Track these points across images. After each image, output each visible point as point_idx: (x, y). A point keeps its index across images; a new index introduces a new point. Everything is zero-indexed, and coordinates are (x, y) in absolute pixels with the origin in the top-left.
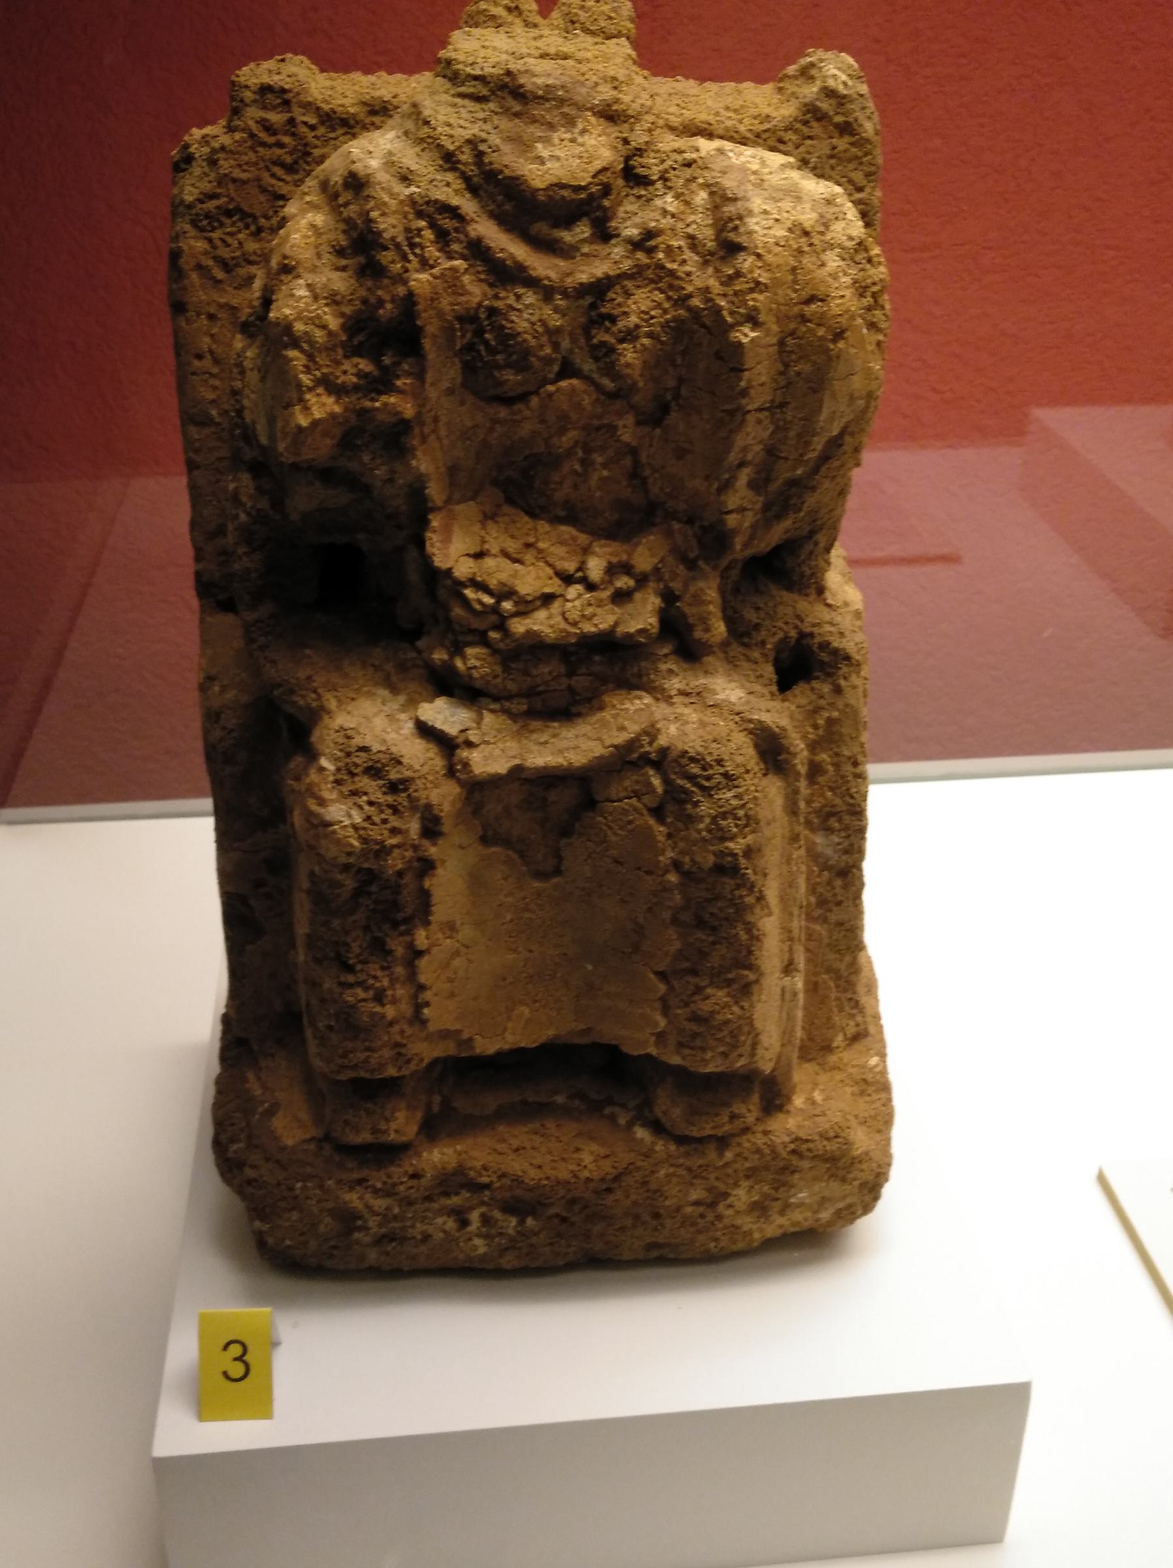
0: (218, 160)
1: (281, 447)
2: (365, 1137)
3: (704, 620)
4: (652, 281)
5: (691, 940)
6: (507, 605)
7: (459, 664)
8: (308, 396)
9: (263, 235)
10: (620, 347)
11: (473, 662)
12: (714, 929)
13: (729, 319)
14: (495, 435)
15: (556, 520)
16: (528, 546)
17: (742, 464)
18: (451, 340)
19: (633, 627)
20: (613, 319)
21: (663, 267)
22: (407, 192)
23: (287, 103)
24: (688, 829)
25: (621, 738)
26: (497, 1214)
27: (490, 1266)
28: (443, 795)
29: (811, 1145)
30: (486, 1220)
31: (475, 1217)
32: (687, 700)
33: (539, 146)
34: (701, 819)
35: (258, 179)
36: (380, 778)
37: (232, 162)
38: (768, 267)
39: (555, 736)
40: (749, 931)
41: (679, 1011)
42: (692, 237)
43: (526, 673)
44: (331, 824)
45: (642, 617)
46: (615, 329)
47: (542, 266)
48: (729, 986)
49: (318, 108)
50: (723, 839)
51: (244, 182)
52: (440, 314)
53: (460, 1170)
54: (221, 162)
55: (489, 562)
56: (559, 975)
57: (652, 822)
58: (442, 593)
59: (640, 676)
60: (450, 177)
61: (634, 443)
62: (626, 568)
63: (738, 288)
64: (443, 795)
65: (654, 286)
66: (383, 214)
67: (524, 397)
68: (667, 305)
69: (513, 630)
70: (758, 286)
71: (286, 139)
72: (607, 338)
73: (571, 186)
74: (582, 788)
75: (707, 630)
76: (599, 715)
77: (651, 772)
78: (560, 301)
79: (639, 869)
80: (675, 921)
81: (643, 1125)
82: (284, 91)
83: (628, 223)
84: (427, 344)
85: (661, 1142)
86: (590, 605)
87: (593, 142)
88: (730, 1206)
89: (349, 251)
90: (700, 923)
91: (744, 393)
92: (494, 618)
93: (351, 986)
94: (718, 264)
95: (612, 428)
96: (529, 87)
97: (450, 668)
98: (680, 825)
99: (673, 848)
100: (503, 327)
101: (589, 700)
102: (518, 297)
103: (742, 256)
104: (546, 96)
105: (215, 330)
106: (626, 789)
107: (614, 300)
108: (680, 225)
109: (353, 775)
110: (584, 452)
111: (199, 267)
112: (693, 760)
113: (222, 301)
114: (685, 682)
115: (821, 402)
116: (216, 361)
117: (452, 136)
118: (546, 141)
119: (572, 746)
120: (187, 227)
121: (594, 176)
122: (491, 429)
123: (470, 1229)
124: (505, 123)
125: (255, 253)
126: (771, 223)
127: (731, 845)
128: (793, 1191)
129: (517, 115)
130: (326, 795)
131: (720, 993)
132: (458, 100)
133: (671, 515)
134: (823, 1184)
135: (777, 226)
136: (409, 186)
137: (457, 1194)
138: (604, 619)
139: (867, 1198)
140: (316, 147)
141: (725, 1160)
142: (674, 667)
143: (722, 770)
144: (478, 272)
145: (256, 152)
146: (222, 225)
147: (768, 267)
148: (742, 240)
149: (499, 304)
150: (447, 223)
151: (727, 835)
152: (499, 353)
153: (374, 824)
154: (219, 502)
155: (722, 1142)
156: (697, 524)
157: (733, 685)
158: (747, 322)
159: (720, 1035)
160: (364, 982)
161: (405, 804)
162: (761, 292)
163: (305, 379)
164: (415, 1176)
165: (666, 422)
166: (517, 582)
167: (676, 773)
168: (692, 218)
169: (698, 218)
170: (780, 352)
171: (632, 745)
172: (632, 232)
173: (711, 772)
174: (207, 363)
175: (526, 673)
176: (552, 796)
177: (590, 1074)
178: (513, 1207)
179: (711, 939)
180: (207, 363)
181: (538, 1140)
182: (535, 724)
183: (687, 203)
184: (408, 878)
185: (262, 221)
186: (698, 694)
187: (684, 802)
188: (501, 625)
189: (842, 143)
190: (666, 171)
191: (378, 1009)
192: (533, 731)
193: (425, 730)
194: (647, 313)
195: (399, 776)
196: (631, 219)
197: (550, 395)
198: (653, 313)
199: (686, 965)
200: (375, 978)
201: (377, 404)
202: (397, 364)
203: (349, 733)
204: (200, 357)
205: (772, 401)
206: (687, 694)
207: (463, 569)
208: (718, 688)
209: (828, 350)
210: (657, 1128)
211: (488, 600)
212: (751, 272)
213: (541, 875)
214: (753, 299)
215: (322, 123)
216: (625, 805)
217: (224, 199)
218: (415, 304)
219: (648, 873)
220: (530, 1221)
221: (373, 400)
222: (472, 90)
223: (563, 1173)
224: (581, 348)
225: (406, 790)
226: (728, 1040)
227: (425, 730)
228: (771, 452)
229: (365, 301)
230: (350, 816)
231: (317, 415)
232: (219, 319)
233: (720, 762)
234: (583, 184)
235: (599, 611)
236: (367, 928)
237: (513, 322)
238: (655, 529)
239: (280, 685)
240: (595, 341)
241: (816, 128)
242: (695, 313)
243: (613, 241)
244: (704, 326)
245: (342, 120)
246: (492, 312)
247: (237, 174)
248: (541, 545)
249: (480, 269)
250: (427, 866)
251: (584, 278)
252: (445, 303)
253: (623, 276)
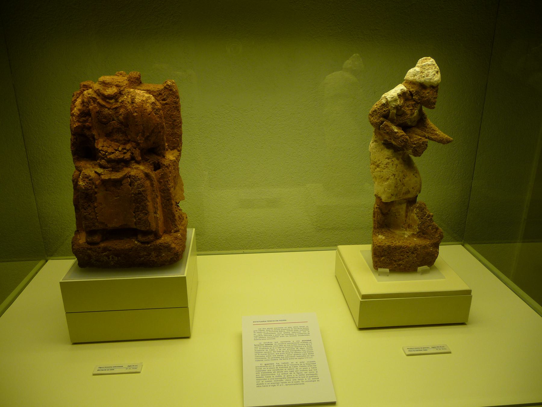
19: (126, 157)
30: (113, 258)
62: (125, 149)
70: (136, 108)
74: (117, 183)
104: (108, 84)
189: (171, 92)
207: (100, 148)
223: (123, 248)
227: (96, 172)
241: (166, 90)
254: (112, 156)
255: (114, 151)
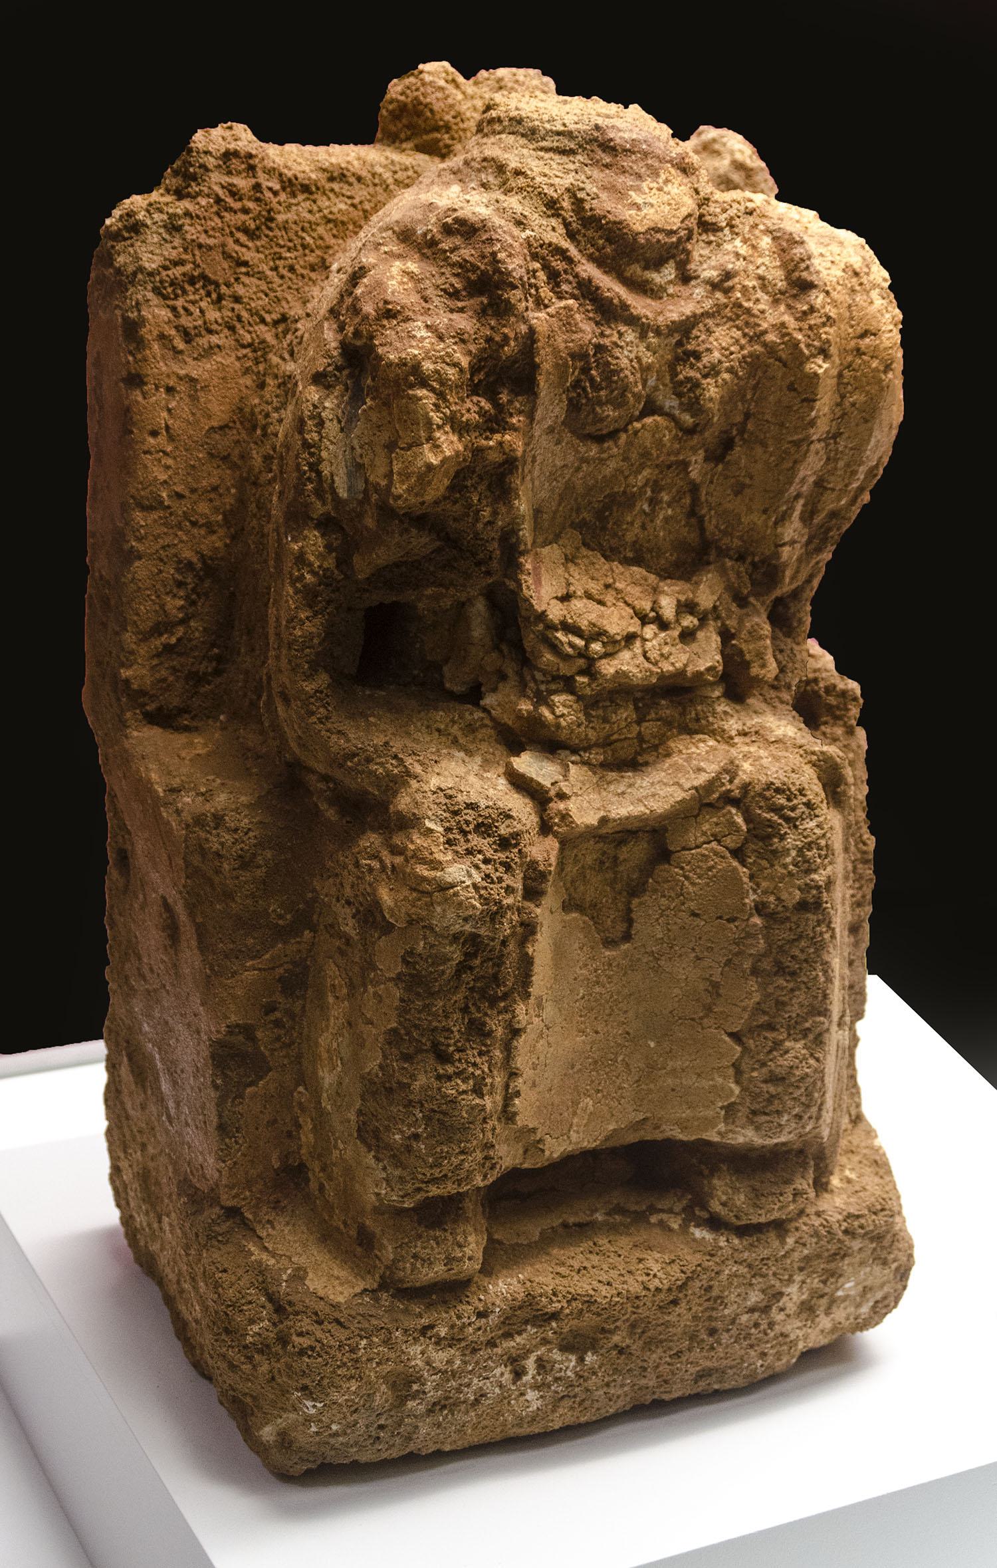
0: (183, 225)
1: (400, 489)
2: (437, 1271)
3: (760, 655)
4: (730, 319)
5: (770, 989)
6: (596, 647)
7: (546, 713)
8: (438, 434)
9: (224, 302)
10: (704, 382)
11: (560, 710)
12: (793, 974)
13: (806, 352)
14: (581, 475)
15: (627, 562)
16: (607, 586)
17: (797, 497)
18: (563, 376)
20: (697, 356)
21: (740, 306)
22: (524, 235)
23: (252, 168)
24: (772, 866)
25: (701, 779)
26: (556, 1355)
27: (536, 1429)
28: (543, 850)
29: (863, 1221)
30: (541, 1364)
31: (530, 1364)
32: (747, 740)
33: (631, 193)
34: (787, 852)
35: (223, 245)
36: (489, 836)
37: (199, 228)
38: (835, 304)
39: (630, 786)
40: (825, 972)
41: (755, 1074)
42: (761, 278)
43: (606, 720)
44: (452, 886)
45: (706, 655)
46: (700, 365)
47: (640, 306)
48: (805, 1036)
49: (281, 175)
50: (808, 871)
51: (210, 248)
52: (556, 351)
53: (531, 1299)
54: (187, 228)
55: (577, 604)
56: (620, 1059)
57: (735, 864)
58: (529, 641)
59: (698, 720)
60: (554, 222)
61: (698, 481)
63: (812, 322)
64: (543, 850)
65: (731, 323)
66: (510, 255)
67: (613, 435)
68: (743, 341)
69: (605, 672)
71: (251, 205)
72: (692, 374)
73: (663, 230)
74: (656, 839)
75: (763, 666)
76: (669, 761)
77: (734, 811)
78: (653, 339)
79: (720, 918)
80: (755, 971)
81: (697, 1226)
82: (250, 156)
83: (705, 266)
84: (542, 380)
85: (723, 1239)
86: (666, 644)
87: (676, 191)
88: (782, 1310)
89: (464, 293)
90: (781, 970)
91: (812, 423)
92: (581, 662)
93: (449, 1078)
94: (790, 302)
95: (685, 465)
96: (618, 141)
97: (535, 721)
98: (764, 863)
99: (755, 891)
100: (609, 364)
101: (655, 747)
102: (621, 335)
103: (814, 293)
105: (172, 405)
106: (704, 833)
107: (698, 337)
108: (751, 267)
109: (465, 833)
110: (653, 492)
111: (162, 337)
112: (778, 791)
113: (182, 372)
114: (740, 723)
115: (871, 430)
116: (171, 439)
117: (552, 185)
118: (638, 189)
119: (652, 793)
120: (150, 295)
121: (682, 222)
122: (578, 469)
123: (525, 1379)
124: (596, 173)
125: (216, 322)
126: (829, 265)
127: (816, 877)
128: (841, 1280)
129: (607, 166)
130: (440, 856)
131: (799, 1045)
132: (542, 154)
133: (723, 553)
134: (868, 1269)
135: (834, 267)
136: (524, 230)
137: (519, 1333)
138: (679, 659)
139: (899, 1287)
140: (279, 212)
141: (787, 1247)
142: (727, 709)
143: (804, 800)
144: (588, 311)
145: (222, 218)
146: (185, 292)
147: (835, 304)
148: (814, 278)
149: (606, 342)
150: (559, 265)
151: (813, 867)
152: (602, 389)
153: (493, 882)
154: (158, 597)
155: (780, 1227)
156: (749, 560)
157: (783, 722)
158: (819, 354)
159: (797, 1093)
160: (462, 1072)
161: (517, 860)
162: (831, 326)
163: (436, 418)
164: (481, 1315)
165: (728, 458)
166: (605, 622)
167: (760, 808)
168: (760, 261)
169: (767, 260)
170: (838, 384)
171: (710, 785)
172: (713, 274)
173: (795, 801)
174: (162, 439)
175: (606, 720)
176: (624, 853)
177: (646, 1175)
178: (574, 1344)
179: (791, 985)
180: (162, 439)
181: (595, 1259)
182: (612, 775)
183: (754, 247)
184: (512, 946)
185: (224, 289)
186: (756, 732)
187: (770, 837)
188: (590, 670)
190: (732, 218)
191: (478, 1101)
192: (609, 783)
193: (520, 783)
194: (727, 349)
195: (510, 830)
196: (708, 262)
197: (636, 433)
198: (732, 349)
199: (764, 1019)
200: (475, 1065)
201: (491, 443)
202: (510, 402)
203: (450, 792)
204: (154, 434)
205: (828, 432)
206: (745, 734)
207: (556, 612)
208: (773, 727)
209: (881, 380)
210: (715, 1223)
211: (580, 642)
212: (824, 307)
213: (609, 943)
214: (826, 333)
215: (284, 189)
216: (705, 851)
217: (189, 267)
218: (534, 341)
219: (732, 920)
220: (590, 1358)
221: (487, 438)
222: (555, 144)
224: (665, 385)
225: (516, 845)
226: (803, 1099)
227: (520, 783)
228: (820, 484)
229: (489, 340)
230: (470, 876)
231: (448, 454)
232: (179, 392)
233: (801, 791)
234: (675, 228)
235: (673, 650)
236: (465, 1010)
237: (617, 358)
238: (712, 567)
239: (355, 755)
240: (681, 377)
242: (771, 349)
243: (693, 283)
244: (779, 360)
245: (302, 185)
246: (599, 348)
247: (203, 239)
248: (619, 585)
249: (590, 308)
250: (529, 929)
251: (675, 317)
252: (560, 340)
253: (706, 314)
254: (627, 663)
255: (634, 626)
